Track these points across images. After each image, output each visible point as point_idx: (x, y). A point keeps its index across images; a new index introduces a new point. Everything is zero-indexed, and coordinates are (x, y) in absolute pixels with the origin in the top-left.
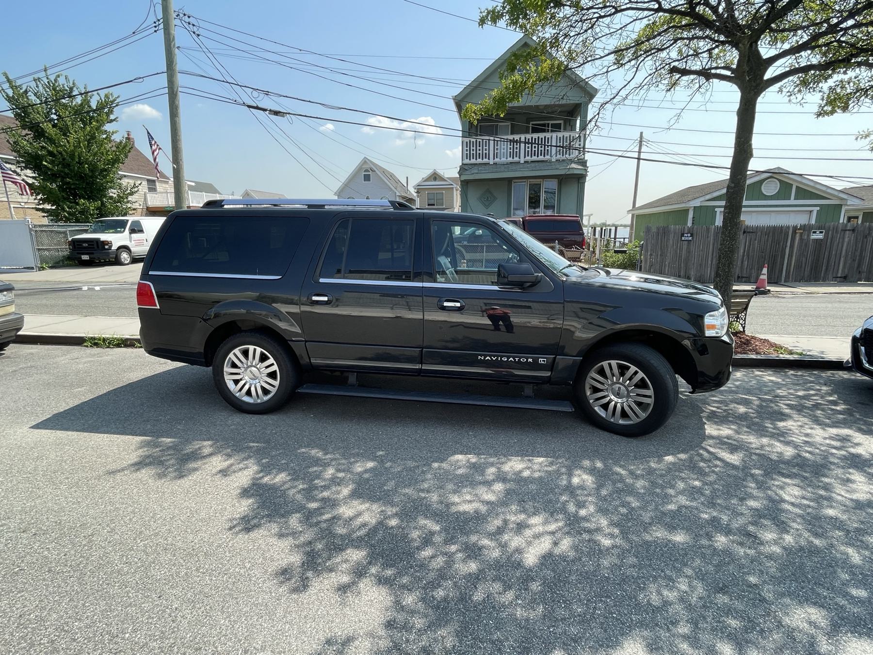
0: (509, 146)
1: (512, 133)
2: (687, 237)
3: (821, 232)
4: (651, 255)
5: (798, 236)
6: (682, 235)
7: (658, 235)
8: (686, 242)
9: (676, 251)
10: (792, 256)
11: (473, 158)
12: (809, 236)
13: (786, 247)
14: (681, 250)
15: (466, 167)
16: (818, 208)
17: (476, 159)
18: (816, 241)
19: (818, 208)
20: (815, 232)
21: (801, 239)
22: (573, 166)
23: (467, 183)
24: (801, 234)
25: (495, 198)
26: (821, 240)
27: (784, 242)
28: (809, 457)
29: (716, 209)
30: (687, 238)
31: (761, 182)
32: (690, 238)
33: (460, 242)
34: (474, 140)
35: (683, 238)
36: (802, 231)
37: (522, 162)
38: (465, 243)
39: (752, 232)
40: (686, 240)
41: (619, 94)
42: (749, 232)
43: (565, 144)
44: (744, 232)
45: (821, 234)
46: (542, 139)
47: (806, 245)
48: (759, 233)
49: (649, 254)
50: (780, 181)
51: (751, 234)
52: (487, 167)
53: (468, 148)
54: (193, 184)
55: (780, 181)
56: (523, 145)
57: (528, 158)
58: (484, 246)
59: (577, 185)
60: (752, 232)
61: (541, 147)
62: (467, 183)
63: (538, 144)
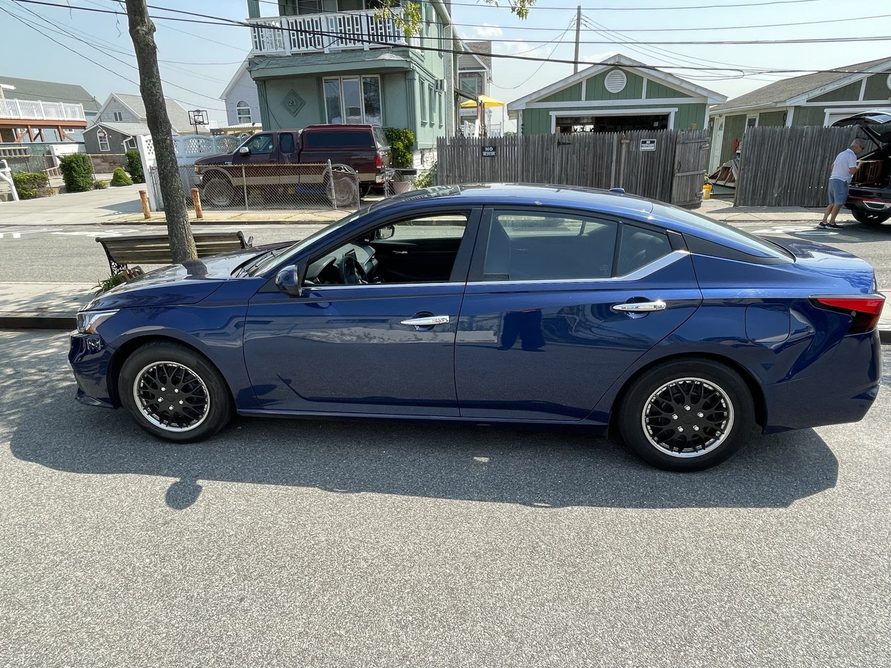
1: (341, 9)
2: (489, 151)
3: (652, 142)
4: (447, 176)
5: (624, 146)
6: (483, 149)
7: (821, 135)
8: (488, 158)
9: (478, 171)
10: (619, 174)
11: (303, 46)
12: (637, 147)
13: (612, 162)
14: (484, 169)
15: (256, 61)
16: (676, 109)
17: (299, 47)
18: (648, 153)
19: (676, 109)
20: (644, 142)
21: (629, 152)
22: (387, 56)
23: (264, 82)
24: (628, 145)
25: (303, 103)
26: (653, 152)
27: (608, 157)
28: (30, 369)
29: (551, 113)
30: (489, 153)
31: (604, 74)
32: (493, 153)
33: (223, 163)
34: (350, 17)
35: (485, 153)
36: (628, 141)
37: (326, 51)
38: (230, 164)
39: (569, 144)
40: (489, 156)
41: (68, 5)
42: (564, 144)
43: (304, 37)
44: (559, 144)
45: (652, 145)
46: (300, 23)
47: (635, 159)
48: (577, 145)
49: (445, 174)
50: (627, 73)
51: (567, 146)
52: (323, 57)
53: (256, 34)
54: (12, 87)
55: (627, 73)
56: (286, 32)
57: (295, 50)
58: (241, 168)
59: (404, 84)
60: (569, 144)
61: (349, 30)
62: (264, 82)
63: (297, 31)
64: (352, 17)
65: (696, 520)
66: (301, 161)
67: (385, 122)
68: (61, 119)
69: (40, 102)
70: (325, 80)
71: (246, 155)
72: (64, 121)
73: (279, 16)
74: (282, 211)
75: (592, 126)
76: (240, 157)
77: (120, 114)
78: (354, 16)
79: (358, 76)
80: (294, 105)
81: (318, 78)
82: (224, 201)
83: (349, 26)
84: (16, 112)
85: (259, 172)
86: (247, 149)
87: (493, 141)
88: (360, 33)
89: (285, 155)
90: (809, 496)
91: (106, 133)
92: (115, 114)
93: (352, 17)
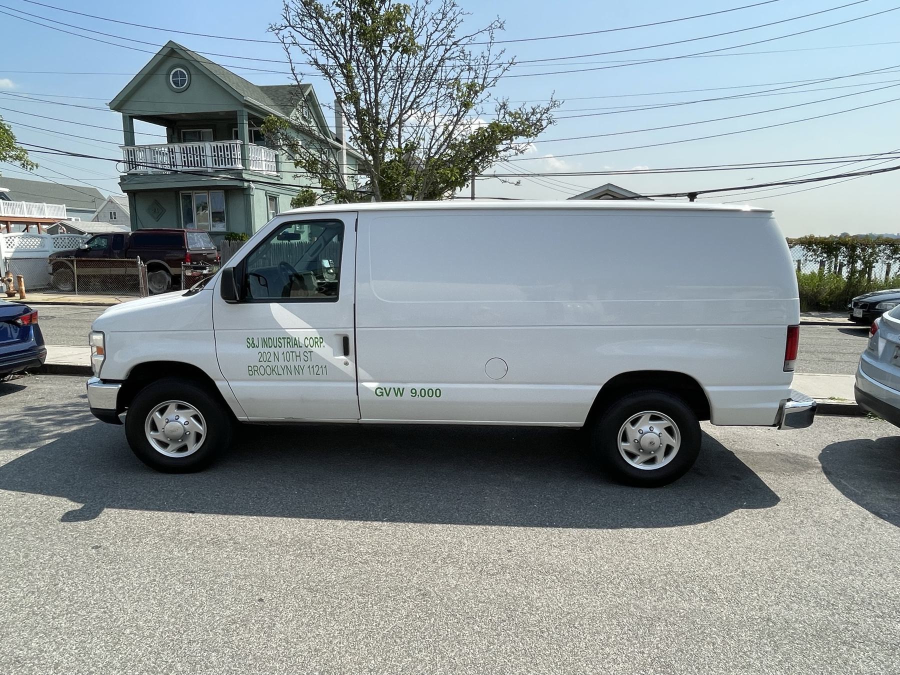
0: (153, 157)
64: (230, 146)
65: (117, 521)
66: (127, 256)
67: (228, 228)
68: (42, 217)
69: (24, 202)
70: (182, 194)
71: (85, 250)
72: (45, 218)
73: (167, 143)
74: (105, 296)
75: (336, 236)
76: (80, 253)
77: (115, 213)
78: (232, 145)
79: (207, 191)
80: (157, 211)
81: (177, 191)
82: (68, 287)
83: (227, 152)
84: (41, 210)
85: (98, 264)
86: (87, 246)
87: (304, 245)
88: (214, 158)
89: (115, 251)
90: (256, 516)
91: (65, 229)
92: (111, 213)
93: (230, 146)
